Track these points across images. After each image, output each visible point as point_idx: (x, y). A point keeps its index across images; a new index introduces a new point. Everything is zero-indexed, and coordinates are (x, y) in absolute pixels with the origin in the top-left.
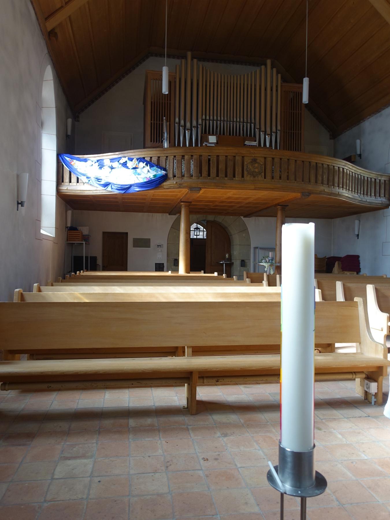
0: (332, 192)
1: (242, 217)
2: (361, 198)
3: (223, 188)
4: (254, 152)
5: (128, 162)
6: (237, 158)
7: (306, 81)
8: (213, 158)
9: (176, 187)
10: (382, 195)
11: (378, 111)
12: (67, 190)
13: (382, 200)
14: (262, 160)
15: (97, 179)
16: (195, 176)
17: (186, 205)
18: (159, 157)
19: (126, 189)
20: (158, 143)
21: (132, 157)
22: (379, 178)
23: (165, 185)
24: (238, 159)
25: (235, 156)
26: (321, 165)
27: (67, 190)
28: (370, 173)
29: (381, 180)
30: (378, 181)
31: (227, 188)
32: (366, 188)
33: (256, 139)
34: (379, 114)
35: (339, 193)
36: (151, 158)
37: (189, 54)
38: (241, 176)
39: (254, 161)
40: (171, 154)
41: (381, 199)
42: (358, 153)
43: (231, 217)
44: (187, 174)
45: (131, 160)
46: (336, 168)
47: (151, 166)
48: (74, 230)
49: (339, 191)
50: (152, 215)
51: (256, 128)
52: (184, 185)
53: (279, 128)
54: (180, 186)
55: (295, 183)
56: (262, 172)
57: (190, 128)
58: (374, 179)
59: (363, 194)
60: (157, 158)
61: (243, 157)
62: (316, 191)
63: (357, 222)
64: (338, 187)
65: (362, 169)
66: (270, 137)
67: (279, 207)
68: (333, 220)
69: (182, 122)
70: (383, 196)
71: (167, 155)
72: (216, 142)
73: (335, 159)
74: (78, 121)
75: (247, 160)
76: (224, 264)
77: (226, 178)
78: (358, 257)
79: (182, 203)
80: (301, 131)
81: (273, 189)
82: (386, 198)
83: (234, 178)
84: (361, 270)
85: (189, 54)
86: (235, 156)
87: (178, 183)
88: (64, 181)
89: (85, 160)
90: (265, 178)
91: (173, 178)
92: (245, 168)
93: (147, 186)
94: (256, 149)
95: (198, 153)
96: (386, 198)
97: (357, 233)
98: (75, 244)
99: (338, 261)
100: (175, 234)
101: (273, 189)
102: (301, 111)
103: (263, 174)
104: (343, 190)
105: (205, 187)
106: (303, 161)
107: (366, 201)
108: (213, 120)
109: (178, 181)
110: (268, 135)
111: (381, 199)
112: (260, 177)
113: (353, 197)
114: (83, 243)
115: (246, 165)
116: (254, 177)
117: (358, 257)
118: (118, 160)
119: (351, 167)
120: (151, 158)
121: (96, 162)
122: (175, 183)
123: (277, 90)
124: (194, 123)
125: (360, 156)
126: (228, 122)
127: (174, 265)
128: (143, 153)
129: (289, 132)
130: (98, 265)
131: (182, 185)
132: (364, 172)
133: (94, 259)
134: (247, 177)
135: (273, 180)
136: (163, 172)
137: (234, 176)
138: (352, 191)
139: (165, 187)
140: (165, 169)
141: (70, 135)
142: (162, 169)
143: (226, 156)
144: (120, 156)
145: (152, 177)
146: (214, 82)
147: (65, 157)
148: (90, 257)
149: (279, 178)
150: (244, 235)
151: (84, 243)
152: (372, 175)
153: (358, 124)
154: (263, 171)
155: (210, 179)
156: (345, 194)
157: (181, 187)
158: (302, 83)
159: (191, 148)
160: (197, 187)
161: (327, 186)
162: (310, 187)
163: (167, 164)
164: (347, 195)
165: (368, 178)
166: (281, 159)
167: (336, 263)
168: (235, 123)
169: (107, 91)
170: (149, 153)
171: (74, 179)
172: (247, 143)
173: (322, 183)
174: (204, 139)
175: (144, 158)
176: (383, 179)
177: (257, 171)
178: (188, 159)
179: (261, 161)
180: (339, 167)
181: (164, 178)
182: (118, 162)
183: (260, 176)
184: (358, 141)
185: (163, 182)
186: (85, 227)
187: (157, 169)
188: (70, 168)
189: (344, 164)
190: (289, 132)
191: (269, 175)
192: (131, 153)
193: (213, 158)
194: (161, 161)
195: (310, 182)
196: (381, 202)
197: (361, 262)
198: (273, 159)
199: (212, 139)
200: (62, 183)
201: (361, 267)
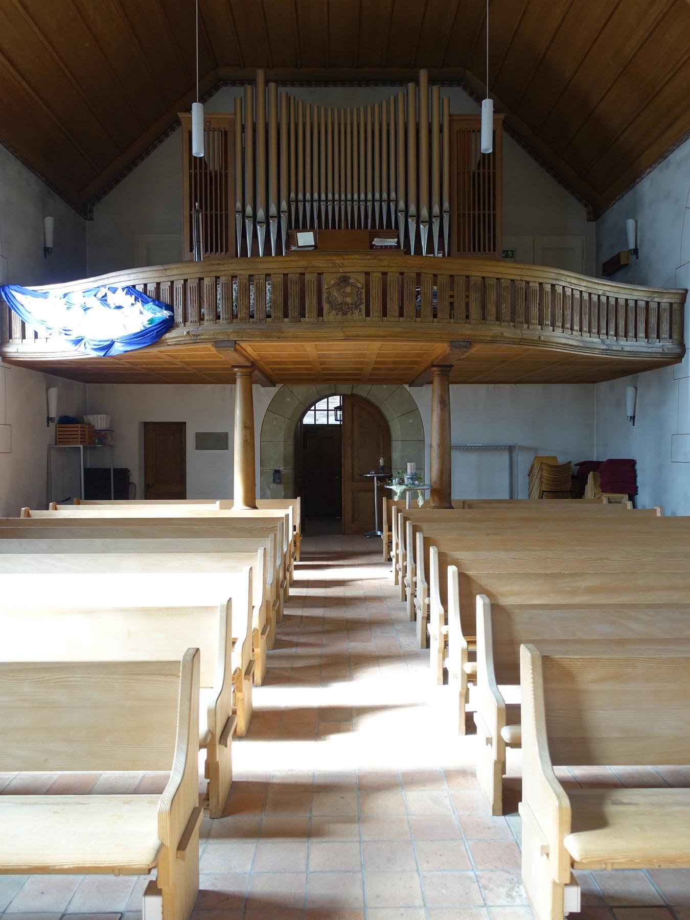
0: (523, 337)
1: (406, 386)
2: (607, 345)
3: (279, 339)
4: (342, 263)
5: (110, 294)
6: (307, 277)
7: (487, 106)
8: (257, 281)
9: (189, 342)
10: (665, 334)
11: (662, 156)
12: (17, 352)
13: (663, 345)
14: (362, 278)
15: (64, 330)
16: (223, 319)
17: (242, 372)
18: (172, 282)
19: (106, 349)
20: (216, 254)
21: (115, 286)
22: (657, 300)
23: (169, 339)
24: (310, 278)
25: (302, 274)
26: (494, 282)
27: (17, 352)
28: (632, 291)
29: (661, 304)
30: (653, 305)
31: (287, 339)
32: (623, 322)
33: (399, 233)
34: (664, 163)
35: (540, 337)
36: (145, 285)
37: (260, 74)
38: (315, 314)
39: (344, 280)
40: (178, 277)
41: (661, 344)
42: (632, 246)
43: (385, 386)
44: (209, 315)
45: (114, 290)
46: (535, 286)
47: (145, 302)
48: (69, 423)
49: (542, 333)
50: (232, 386)
51: (398, 211)
52: (202, 337)
53: (446, 205)
54: (196, 339)
55: (433, 322)
56: (361, 303)
57: (439, 214)
58: (644, 303)
59: (616, 335)
60: (197, 281)
61: (320, 274)
62: (482, 336)
63: (630, 391)
64: (539, 325)
65: (617, 285)
66: (427, 227)
67: (435, 369)
68: (596, 385)
69: (249, 210)
70: (667, 336)
71: (172, 279)
72: (313, 244)
73: (533, 268)
74: (91, 219)
75: (329, 281)
76: (375, 478)
77: (286, 320)
78: (632, 463)
79: (237, 369)
80: (494, 210)
81: (383, 337)
82: (674, 341)
83: (302, 319)
84: (639, 489)
85: (260, 74)
86: (302, 274)
87: (191, 334)
88: (14, 336)
89: (45, 295)
90: (368, 314)
91: (183, 324)
92: (324, 296)
93: (139, 342)
94: (345, 257)
95: (229, 271)
96: (674, 341)
97: (630, 414)
98: (67, 449)
99: (594, 470)
100: (274, 423)
101: (383, 337)
102: (494, 168)
103: (363, 307)
104: (553, 331)
105: (243, 339)
106: (452, 276)
107: (622, 351)
108: (389, 201)
109: (190, 330)
110: (425, 224)
111: (661, 344)
112: (357, 314)
113: (581, 344)
114: (80, 448)
115: (328, 290)
116: (344, 314)
117: (632, 463)
118: (94, 293)
119: (574, 281)
120: (145, 285)
121: (60, 298)
122: (185, 333)
123: (441, 131)
124: (273, 210)
125: (636, 251)
126: (329, 203)
127: (274, 482)
128: (132, 277)
129: (469, 215)
130: (133, 483)
131: (199, 338)
132: (615, 290)
133: (123, 475)
134: (330, 316)
135: (385, 319)
136: (166, 314)
137: (303, 315)
138: (581, 330)
139: (170, 342)
140: (170, 308)
141: (51, 248)
142: (164, 308)
143: (286, 275)
144: (96, 285)
145: (146, 323)
146: (339, 124)
147: (11, 290)
148: (114, 469)
149: (397, 313)
150: (411, 421)
151: (81, 446)
152: (635, 293)
153: (633, 187)
154: (364, 300)
155: (253, 322)
156: (558, 339)
157: (198, 341)
158: (189, 110)
159: (269, 259)
160: (227, 339)
161: (512, 324)
162: (467, 330)
163: (218, 293)
164: (564, 341)
165: (626, 300)
166: (402, 274)
167: (590, 476)
168: (357, 202)
169: (143, 159)
170: (141, 275)
171: (29, 333)
172: (377, 242)
173: (498, 318)
174: (291, 240)
175: (134, 286)
176: (665, 300)
177: (350, 302)
178: (210, 284)
179: (358, 280)
180: (541, 284)
181: (168, 325)
182: (95, 296)
183: (357, 312)
184: (631, 223)
185: (166, 332)
186: (99, 416)
187: (154, 307)
188: (21, 312)
189: (553, 276)
190: (469, 215)
191: (376, 306)
192: (113, 278)
193: (257, 281)
194: (161, 292)
195: (467, 317)
196: (661, 350)
197: (638, 473)
198: (385, 274)
199: (306, 239)
200: (10, 340)
201: (638, 484)
